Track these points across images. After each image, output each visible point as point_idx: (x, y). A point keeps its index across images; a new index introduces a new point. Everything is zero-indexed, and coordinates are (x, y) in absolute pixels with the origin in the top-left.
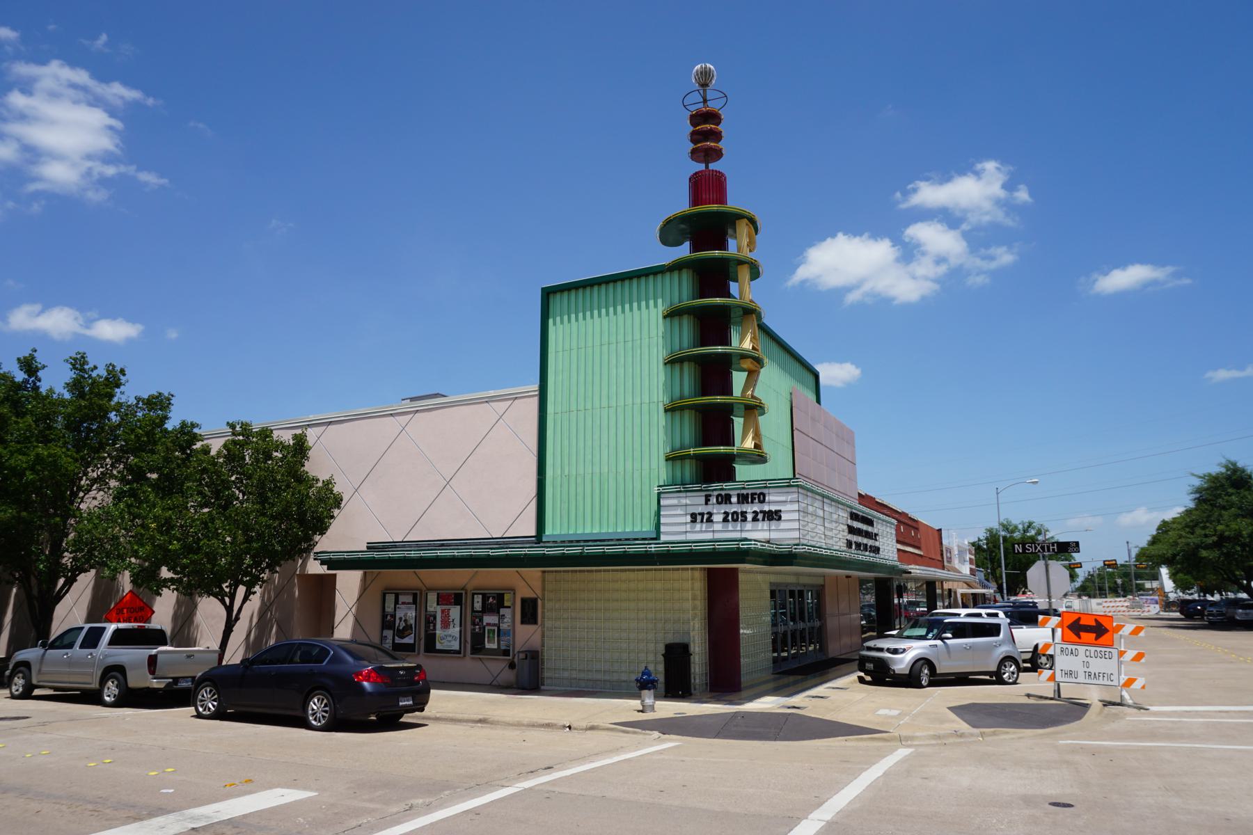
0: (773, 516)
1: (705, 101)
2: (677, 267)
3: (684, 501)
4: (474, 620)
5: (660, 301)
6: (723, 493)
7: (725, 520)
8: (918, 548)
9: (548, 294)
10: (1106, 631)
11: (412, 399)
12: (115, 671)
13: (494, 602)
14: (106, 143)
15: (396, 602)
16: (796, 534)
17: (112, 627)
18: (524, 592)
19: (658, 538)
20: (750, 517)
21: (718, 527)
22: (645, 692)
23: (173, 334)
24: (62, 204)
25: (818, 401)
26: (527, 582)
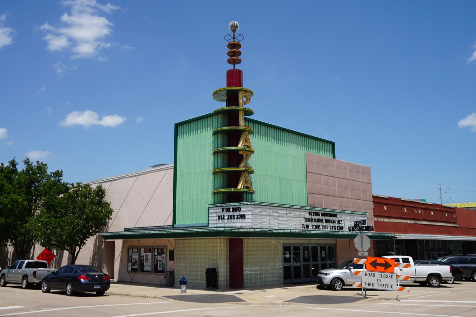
0: (243, 217)
1: (234, 38)
2: (217, 113)
3: (217, 211)
4: (154, 259)
5: (211, 128)
6: (228, 207)
7: (228, 218)
8: (455, 223)
9: (177, 126)
10: (391, 266)
11: (154, 167)
12: (25, 277)
13: (161, 251)
14: (106, 31)
15: (132, 252)
16: (250, 224)
17: (27, 261)
18: (170, 248)
19: (208, 226)
20: (236, 217)
21: (226, 221)
22: (182, 286)
23: (140, 120)
24: (86, 63)
25: (334, 157)
26: (170, 243)
